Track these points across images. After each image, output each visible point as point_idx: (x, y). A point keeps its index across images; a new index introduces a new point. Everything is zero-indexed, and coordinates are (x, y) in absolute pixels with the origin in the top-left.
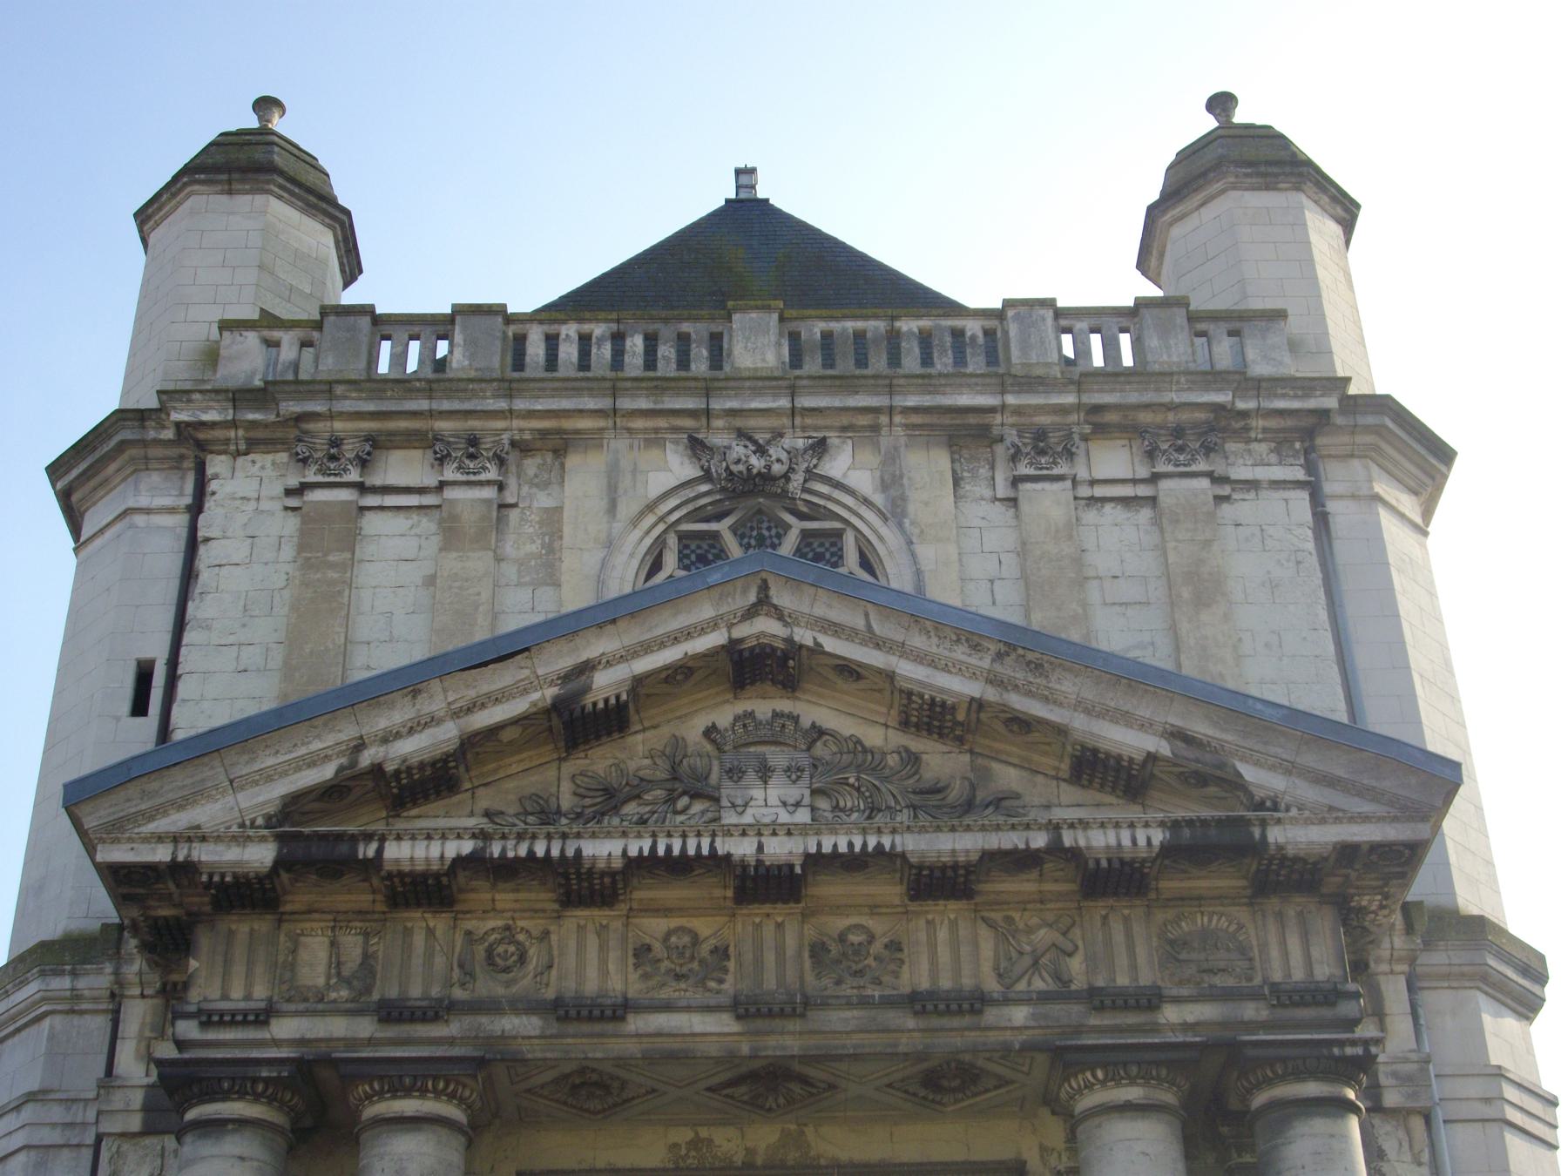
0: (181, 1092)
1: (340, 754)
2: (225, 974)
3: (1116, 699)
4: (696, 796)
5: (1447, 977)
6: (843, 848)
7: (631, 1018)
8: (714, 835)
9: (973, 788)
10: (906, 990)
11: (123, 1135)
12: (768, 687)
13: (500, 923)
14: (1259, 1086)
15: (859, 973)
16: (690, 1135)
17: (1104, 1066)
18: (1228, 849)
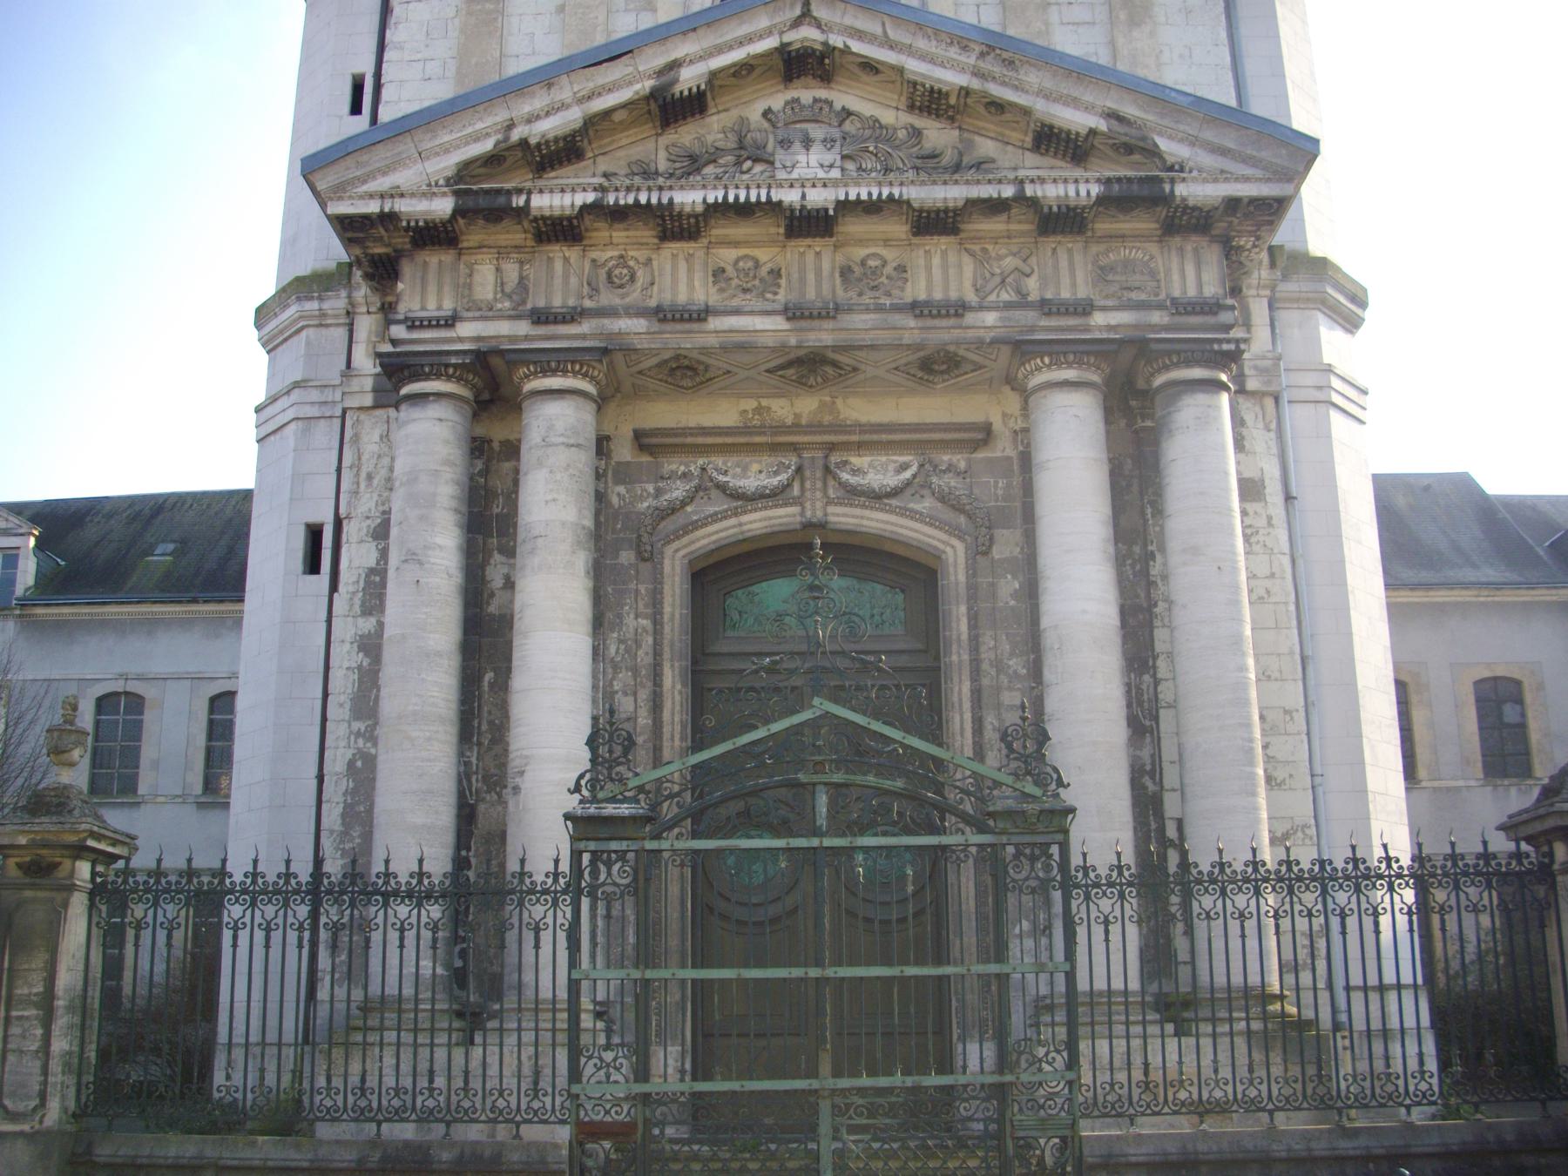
0: (398, 372)
1: (497, 132)
2: (425, 290)
3: (1066, 87)
4: (756, 160)
5: (1297, 300)
6: (864, 197)
7: (710, 319)
8: (769, 187)
9: (961, 154)
10: (909, 300)
11: (360, 409)
12: (809, 80)
13: (616, 253)
14: (1159, 371)
15: (874, 288)
16: (754, 404)
17: (1050, 355)
18: (1146, 198)
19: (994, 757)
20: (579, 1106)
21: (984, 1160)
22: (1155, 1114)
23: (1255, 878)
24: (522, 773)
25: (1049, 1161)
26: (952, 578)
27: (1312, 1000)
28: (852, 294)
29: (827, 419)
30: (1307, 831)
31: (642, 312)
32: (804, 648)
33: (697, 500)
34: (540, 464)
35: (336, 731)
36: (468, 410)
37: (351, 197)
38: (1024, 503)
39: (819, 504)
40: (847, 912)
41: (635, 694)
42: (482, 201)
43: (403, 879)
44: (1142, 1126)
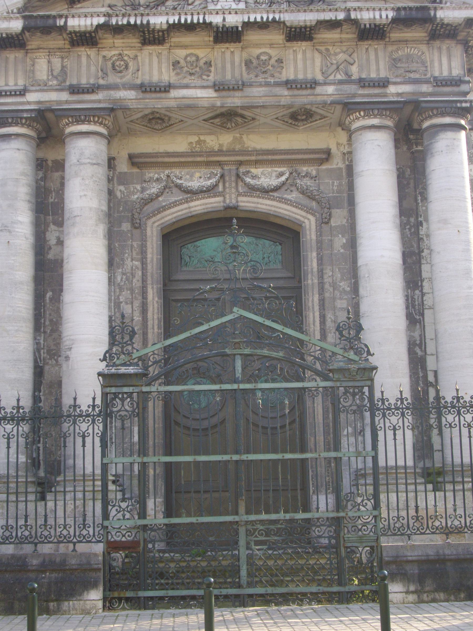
6: (259, 19)
7: (172, 91)
8: (205, 14)
10: (284, 79)
13: (117, 52)
14: (426, 119)
15: (265, 72)
16: (197, 139)
17: (364, 110)
19: (332, 337)
20: (108, 532)
21: (329, 559)
22: (422, 534)
24: (70, 349)
25: (364, 560)
26: (308, 237)
28: (252, 76)
29: (238, 147)
32: (228, 276)
33: (165, 194)
36: (34, 144)
38: (349, 195)
39: (233, 196)
41: (132, 303)
44: (415, 541)
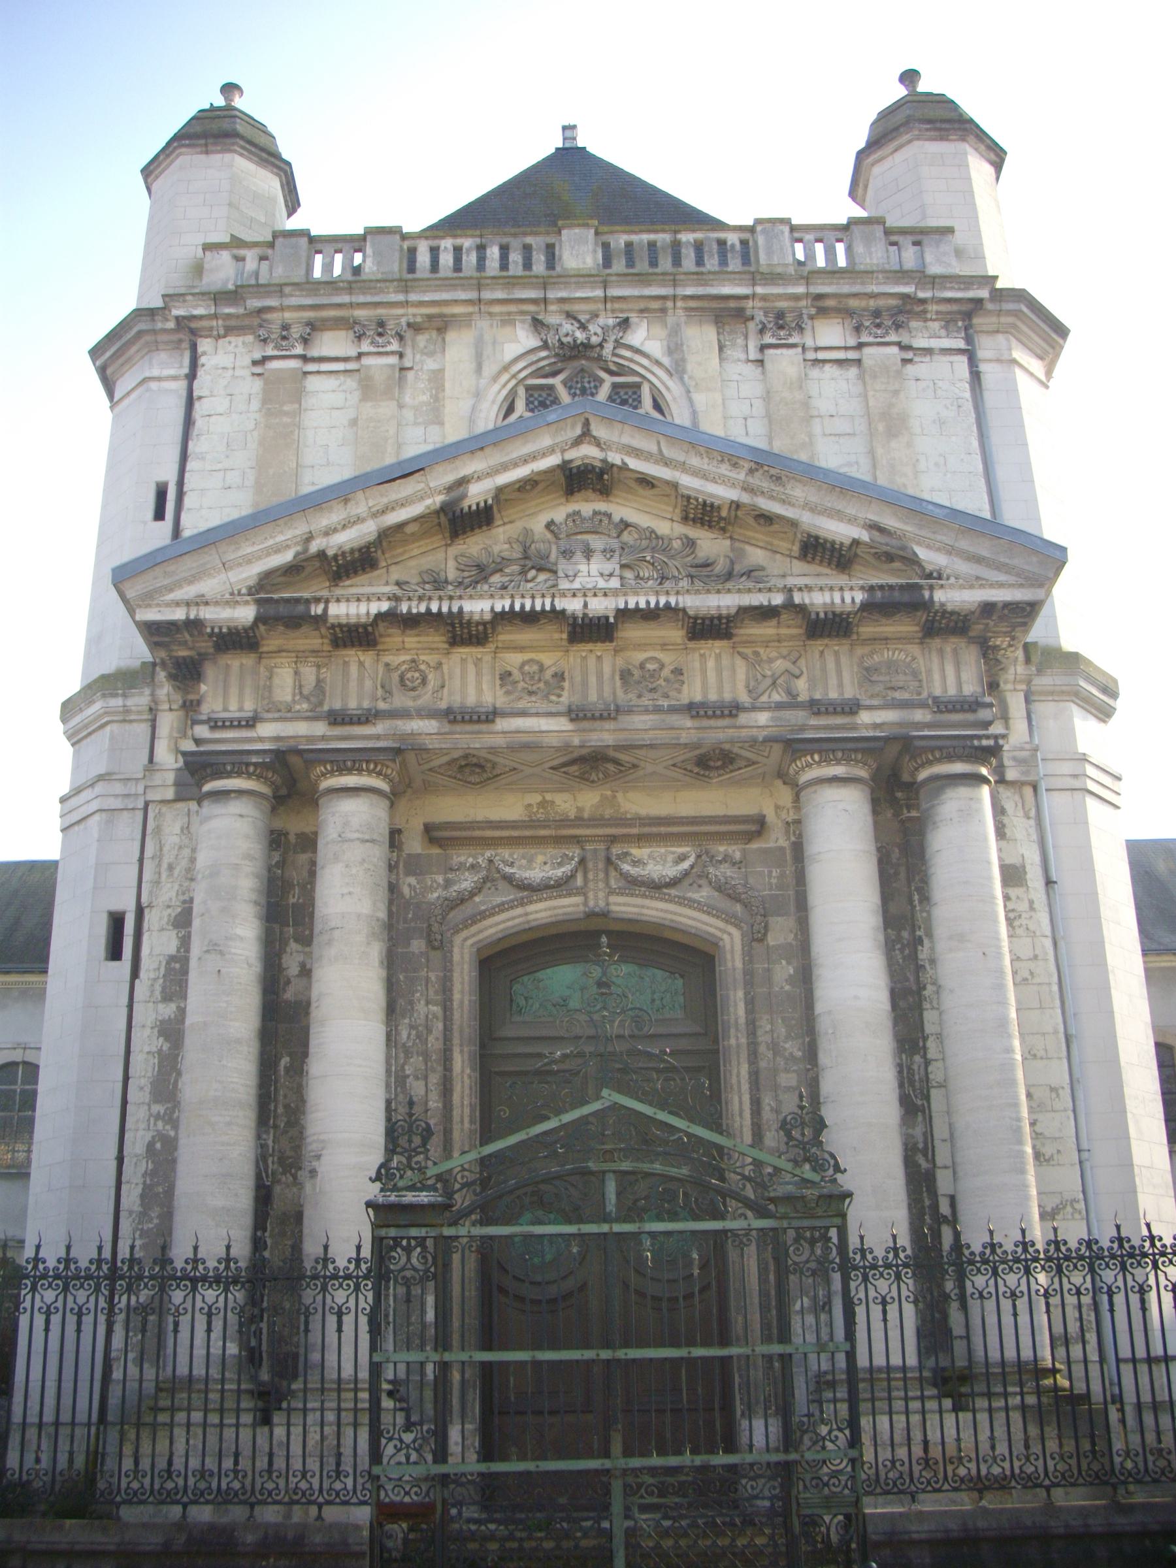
0: (200, 772)
1: (297, 543)
2: (226, 691)
4: (540, 569)
5: (1052, 693)
6: (642, 605)
7: (498, 720)
8: (553, 596)
9: (732, 563)
10: (686, 701)
11: (162, 802)
12: (590, 493)
13: (408, 658)
14: (923, 765)
17: (820, 752)
18: (907, 604)
19: (772, 1138)
20: (379, 1487)
22: (935, 1490)
23: (1024, 1258)
24: (318, 1157)
25: (834, 1538)
26: (729, 965)
27: (1083, 1374)
29: (608, 813)
30: (1076, 1206)
31: (433, 714)
33: (485, 891)
34: (336, 858)
35: (137, 1114)
36: (266, 805)
37: (158, 605)
39: (601, 895)
40: (637, 1292)
41: (426, 1078)
42: (283, 610)
43: (211, 1264)
